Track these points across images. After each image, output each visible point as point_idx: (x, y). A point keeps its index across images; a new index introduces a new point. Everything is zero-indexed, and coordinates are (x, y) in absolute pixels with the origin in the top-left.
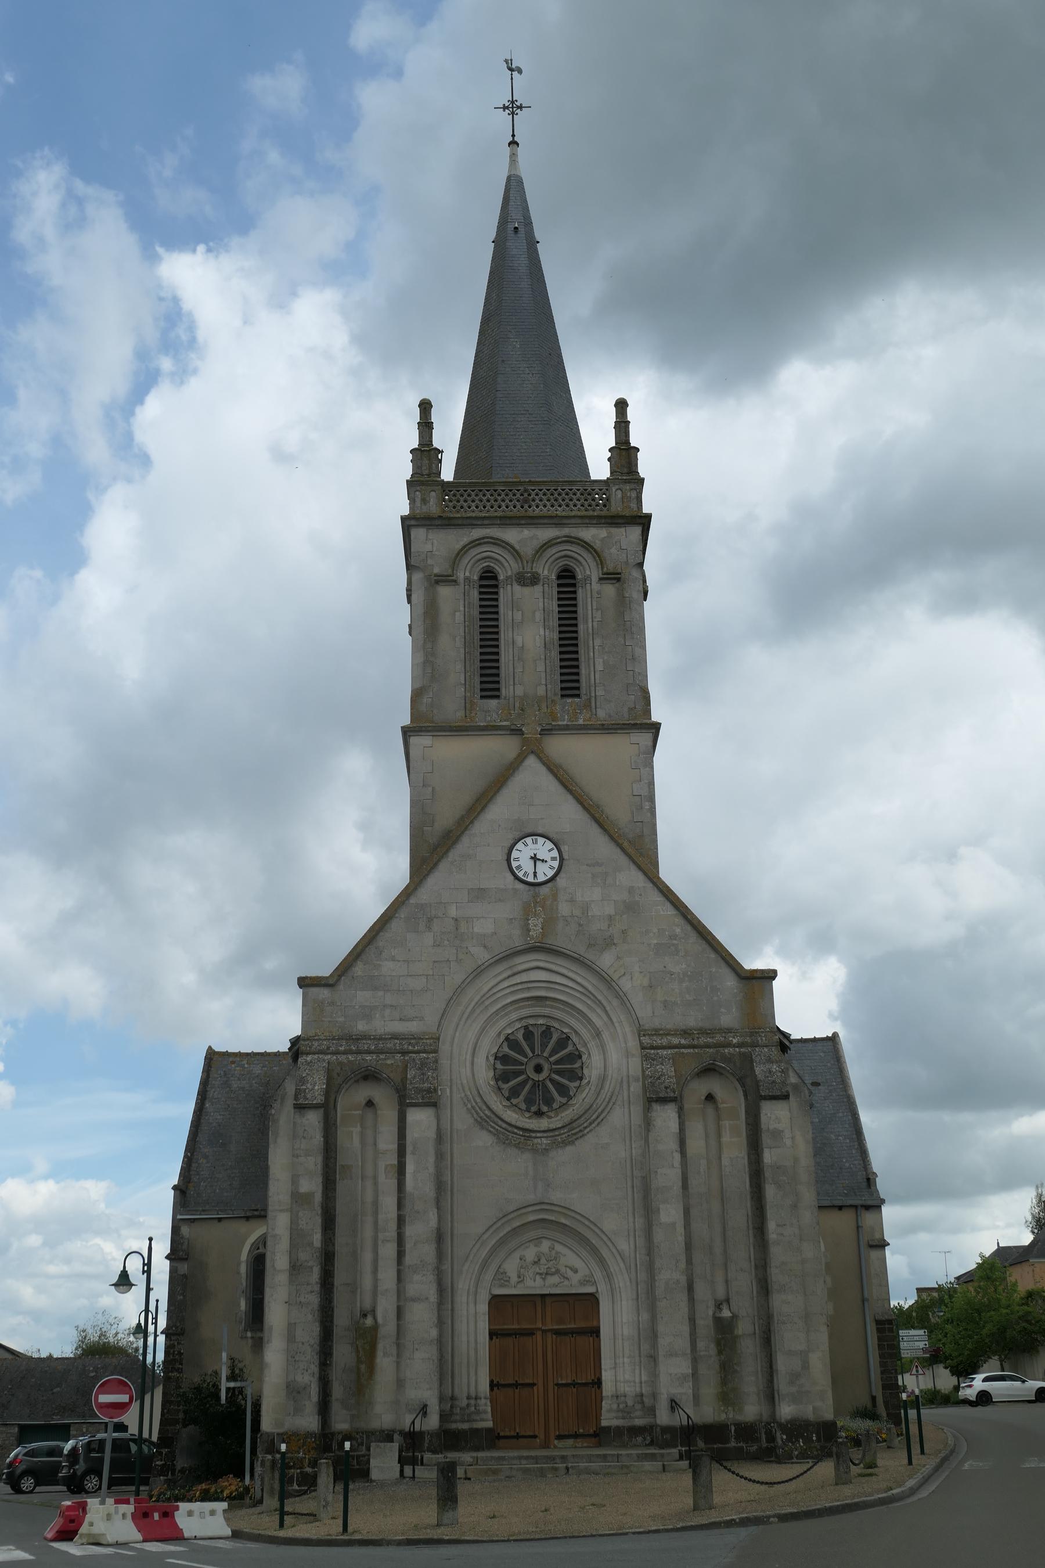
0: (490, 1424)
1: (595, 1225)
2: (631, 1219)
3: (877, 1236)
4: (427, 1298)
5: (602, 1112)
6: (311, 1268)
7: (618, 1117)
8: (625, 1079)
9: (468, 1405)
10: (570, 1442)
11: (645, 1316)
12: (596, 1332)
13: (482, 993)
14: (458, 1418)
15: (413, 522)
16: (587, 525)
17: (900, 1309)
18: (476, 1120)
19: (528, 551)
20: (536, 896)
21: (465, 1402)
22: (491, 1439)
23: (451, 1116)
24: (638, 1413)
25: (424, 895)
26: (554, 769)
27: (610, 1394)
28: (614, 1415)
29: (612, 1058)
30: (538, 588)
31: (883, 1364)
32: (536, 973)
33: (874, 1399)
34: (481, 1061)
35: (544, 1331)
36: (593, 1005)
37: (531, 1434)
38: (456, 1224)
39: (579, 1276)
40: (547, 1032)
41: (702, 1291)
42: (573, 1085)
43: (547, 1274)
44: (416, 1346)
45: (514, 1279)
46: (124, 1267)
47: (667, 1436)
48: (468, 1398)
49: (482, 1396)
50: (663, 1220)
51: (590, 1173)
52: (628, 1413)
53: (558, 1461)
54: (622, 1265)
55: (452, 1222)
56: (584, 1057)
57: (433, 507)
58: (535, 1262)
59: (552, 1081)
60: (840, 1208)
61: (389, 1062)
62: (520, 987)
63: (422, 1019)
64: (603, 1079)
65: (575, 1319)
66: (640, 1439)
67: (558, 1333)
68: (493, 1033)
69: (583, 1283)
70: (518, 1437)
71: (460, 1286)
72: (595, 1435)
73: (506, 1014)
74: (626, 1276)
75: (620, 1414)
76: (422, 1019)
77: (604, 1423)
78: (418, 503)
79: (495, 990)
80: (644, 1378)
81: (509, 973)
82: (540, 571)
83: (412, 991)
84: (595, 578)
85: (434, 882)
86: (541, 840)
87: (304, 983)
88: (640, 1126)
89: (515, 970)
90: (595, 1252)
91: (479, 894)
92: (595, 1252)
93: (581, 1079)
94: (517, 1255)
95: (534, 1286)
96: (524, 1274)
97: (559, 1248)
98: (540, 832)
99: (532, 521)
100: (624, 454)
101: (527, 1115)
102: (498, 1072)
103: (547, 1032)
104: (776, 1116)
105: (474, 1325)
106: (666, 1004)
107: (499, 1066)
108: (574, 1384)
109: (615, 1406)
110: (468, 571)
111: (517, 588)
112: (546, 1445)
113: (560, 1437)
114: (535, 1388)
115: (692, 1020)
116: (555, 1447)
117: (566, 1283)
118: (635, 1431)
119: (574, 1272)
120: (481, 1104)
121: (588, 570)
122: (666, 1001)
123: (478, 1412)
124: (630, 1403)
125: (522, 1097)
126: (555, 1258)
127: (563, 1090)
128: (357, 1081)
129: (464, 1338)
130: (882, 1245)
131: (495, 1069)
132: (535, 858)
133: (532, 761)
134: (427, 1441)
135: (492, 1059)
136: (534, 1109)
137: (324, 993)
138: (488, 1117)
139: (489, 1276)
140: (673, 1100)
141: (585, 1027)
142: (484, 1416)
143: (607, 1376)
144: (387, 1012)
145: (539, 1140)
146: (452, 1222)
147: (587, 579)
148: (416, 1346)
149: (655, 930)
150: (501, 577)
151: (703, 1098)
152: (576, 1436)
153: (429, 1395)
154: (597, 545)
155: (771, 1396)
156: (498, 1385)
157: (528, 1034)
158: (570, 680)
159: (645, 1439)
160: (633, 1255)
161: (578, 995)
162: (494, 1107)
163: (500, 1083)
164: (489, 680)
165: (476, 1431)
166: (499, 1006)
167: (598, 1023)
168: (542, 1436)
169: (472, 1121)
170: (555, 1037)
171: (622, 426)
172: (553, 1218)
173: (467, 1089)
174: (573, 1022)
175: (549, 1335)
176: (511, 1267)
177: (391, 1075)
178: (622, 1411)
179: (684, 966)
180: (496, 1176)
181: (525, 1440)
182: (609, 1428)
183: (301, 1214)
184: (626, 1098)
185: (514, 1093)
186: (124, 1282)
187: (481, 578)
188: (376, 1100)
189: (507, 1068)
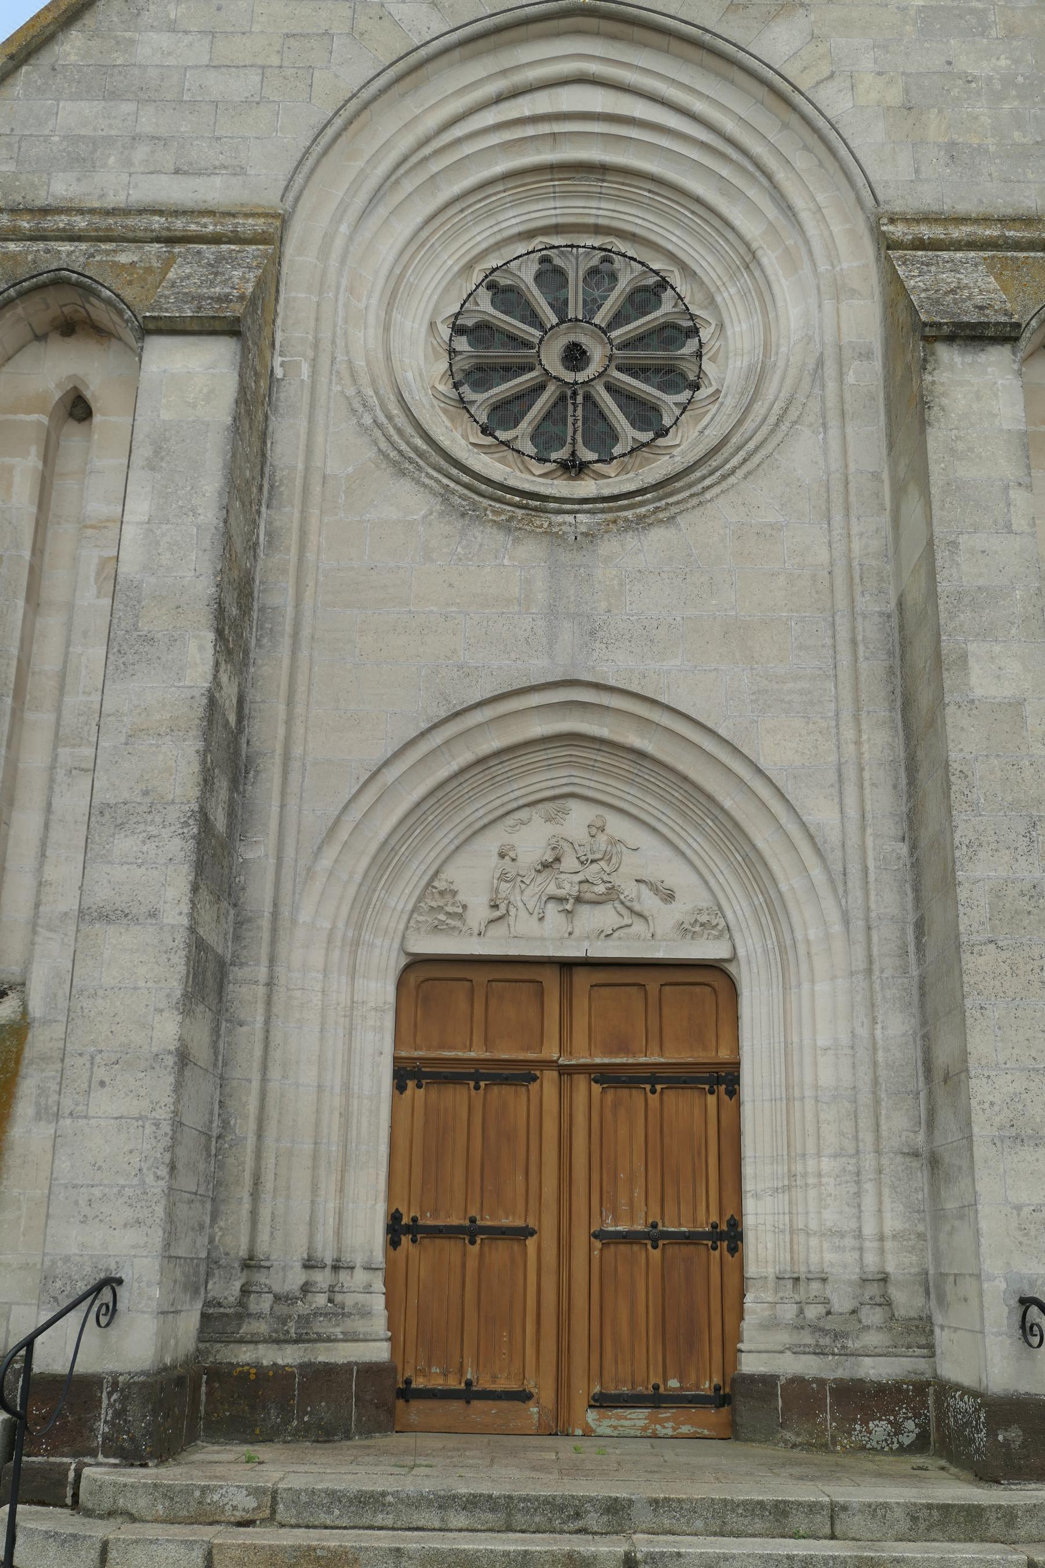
0: (379, 1352)
1: (736, 750)
2: (848, 733)
4: (153, 914)
5: (757, 449)
7: (804, 456)
8: (830, 352)
9: (306, 1289)
10: (637, 1418)
11: (896, 1026)
12: (725, 1079)
14: (262, 1327)
21: (296, 1278)
22: (376, 1403)
23: (310, 433)
24: (873, 1339)
27: (770, 1271)
28: (784, 1338)
35: (566, 1072)
37: (514, 1386)
38: (299, 730)
42: (669, 401)
43: (578, 900)
44: (100, 1073)
45: (479, 913)
47: (1011, 1435)
48: (310, 1264)
49: (359, 1260)
50: (978, 692)
51: (725, 600)
52: (837, 1336)
53: (593, 1520)
54: (817, 873)
55: (289, 722)
56: (705, 334)
58: (546, 866)
61: (124, 258)
62: (530, 131)
63: (240, 171)
64: (758, 378)
65: (665, 1036)
66: (880, 1429)
67: (608, 1077)
68: (451, 257)
69: (685, 931)
70: (468, 1394)
71: (305, 916)
72: (721, 1399)
74: (829, 905)
75: (808, 1339)
76: (240, 171)
77: (750, 1365)
79: (458, 131)
80: (892, 1223)
81: (500, 85)
83: (216, 103)
88: (876, 476)
90: (731, 833)
93: (696, 387)
94: (491, 842)
96: (506, 903)
97: (617, 826)
102: (462, 364)
105: (333, 1048)
106: (952, 152)
108: (654, 1237)
109: (789, 1312)
112: (557, 1426)
113: (603, 1402)
114: (531, 1242)
116: (588, 1433)
117: (639, 927)
118: (859, 1399)
119: (662, 899)
120: (401, 420)
122: (953, 144)
123: (338, 1312)
124: (842, 1303)
125: (526, 426)
126: (607, 857)
127: (645, 414)
128: (40, 337)
129: (309, 1075)
131: (452, 352)
134: (106, 1413)
135: (445, 331)
136: (562, 454)
138: (421, 454)
141: (711, 248)
142: (358, 1325)
143: (759, 1214)
144: (141, 152)
145: (569, 518)
146: (289, 722)
148: (100, 1073)
152: (656, 1400)
153: (131, 1244)
156: (415, 1229)
159: (898, 1429)
160: (853, 839)
161: (694, 154)
162: (444, 441)
163: (465, 389)
165: (323, 1377)
168: (547, 1395)
169: (371, 453)
170: (624, 282)
172: (605, 732)
173: (364, 380)
174: (674, 238)
175: (581, 1083)
176: (473, 877)
177: (128, 294)
178: (816, 1329)
179: (1003, 62)
180: (418, 599)
181: (493, 1408)
182: (768, 1381)
184: (832, 401)
185: (505, 413)
188: (95, 390)
189: (488, 353)
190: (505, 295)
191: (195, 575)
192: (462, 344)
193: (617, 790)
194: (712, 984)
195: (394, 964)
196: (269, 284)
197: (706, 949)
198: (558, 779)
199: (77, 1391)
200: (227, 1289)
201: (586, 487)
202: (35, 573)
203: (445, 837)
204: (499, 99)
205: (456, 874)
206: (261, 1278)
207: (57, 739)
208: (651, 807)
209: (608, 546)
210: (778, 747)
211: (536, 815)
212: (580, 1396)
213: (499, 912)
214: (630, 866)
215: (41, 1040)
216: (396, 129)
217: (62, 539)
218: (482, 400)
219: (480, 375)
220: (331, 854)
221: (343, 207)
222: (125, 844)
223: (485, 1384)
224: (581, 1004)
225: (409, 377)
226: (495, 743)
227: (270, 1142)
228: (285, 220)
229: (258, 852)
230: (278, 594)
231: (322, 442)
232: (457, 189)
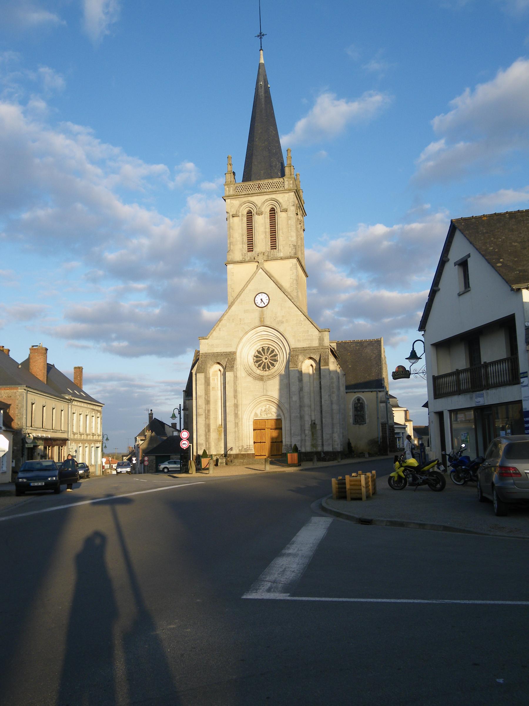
17: (336, 424)
20: (262, 311)
30: (263, 216)
45: (259, 415)
46: (413, 348)
91: (246, 311)
97: (271, 407)
99: (261, 194)
121: (278, 210)
143: (284, 440)
155: (323, 445)
157: (263, 350)
158: (274, 245)
185: (259, 366)
189: (258, 359)
192: (255, 358)
195: (253, 420)
209: (268, 382)
218: (257, 364)
219: (257, 362)
225: (250, 364)
229: (239, 413)
231: (241, 373)
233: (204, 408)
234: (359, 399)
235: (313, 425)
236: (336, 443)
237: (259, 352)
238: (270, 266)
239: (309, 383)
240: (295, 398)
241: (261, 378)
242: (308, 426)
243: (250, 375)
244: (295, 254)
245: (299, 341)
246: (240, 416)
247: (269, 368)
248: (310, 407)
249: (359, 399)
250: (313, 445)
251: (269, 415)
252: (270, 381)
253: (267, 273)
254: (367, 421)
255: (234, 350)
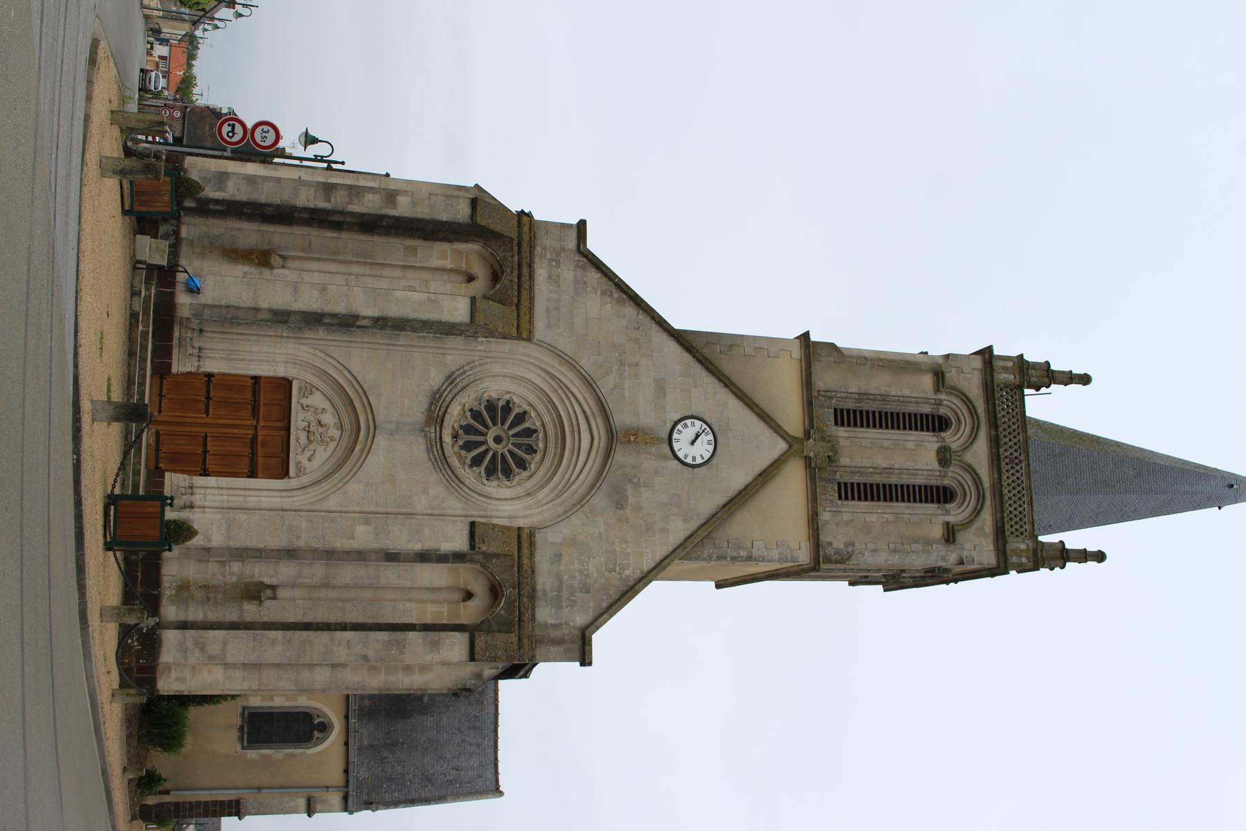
0: (174, 369)
3: (319, 806)
6: (330, 201)
7: (454, 505)
12: (253, 474)
13: (570, 386)
15: (987, 356)
16: (994, 514)
18: (453, 373)
19: (969, 457)
20: (659, 439)
21: (197, 345)
25: (659, 337)
26: (775, 466)
29: (507, 504)
30: (936, 466)
31: (198, 803)
32: (589, 439)
33: (167, 792)
34: (507, 385)
35: (256, 427)
36: (556, 491)
39: (305, 462)
40: (531, 450)
41: (285, 571)
45: (305, 402)
48: (200, 349)
57: (1003, 377)
58: (320, 422)
59: (487, 451)
60: (346, 771)
65: (266, 455)
67: (254, 439)
68: (532, 398)
69: (299, 463)
70: (161, 396)
71: (302, 347)
72: (157, 467)
73: (549, 411)
78: (1001, 363)
79: (572, 399)
81: (589, 413)
82: (952, 468)
84: (948, 519)
85: (672, 347)
86: (711, 448)
87: (582, 225)
89: (591, 418)
90: (328, 476)
91: (660, 389)
92: (328, 476)
94: (328, 406)
95: (298, 420)
96: (311, 410)
97: (333, 445)
98: (719, 448)
100: (1062, 556)
101: (456, 426)
103: (531, 450)
104: (455, 647)
105: (264, 357)
107: (501, 403)
108: (205, 452)
110: (949, 405)
111: (935, 446)
113: (158, 434)
115: (544, 581)
121: (956, 513)
126: (322, 441)
128: (492, 267)
129: (255, 349)
130: (310, 812)
132: (692, 445)
133: (782, 446)
137: (572, 244)
139: (311, 379)
140: (472, 547)
143: (211, 481)
147: (948, 513)
149: (629, 550)
150: (943, 434)
151: (469, 588)
152: (157, 449)
154: (977, 524)
155: (184, 626)
156: (209, 381)
157: (530, 432)
164: (849, 417)
166: (556, 402)
167: (541, 495)
168: (159, 418)
169: (453, 369)
171: (1083, 556)
174: (541, 473)
175: (252, 432)
176: (317, 400)
180: (400, 382)
183: (378, 196)
186: (310, 140)
187: (940, 418)
189: (498, 411)
190: (522, 417)
191: (394, 311)
193: (344, 445)
194: (284, 473)
196: (523, 339)
197: (292, 470)
198: (347, 426)
199: (172, 284)
200: (195, 323)
201: (447, 439)
202: (413, 267)
203: (329, 391)
204: (584, 412)
205: (318, 394)
206: (196, 334)
207: (357, 275)
208: (338, 454)
209: (422, 441)
210: (352, 487)
211: (336, 420)
212: (162, 428)
213: (305, 408)
214: (320, 449)
215: (266, 272)
216: (568, 377)
217: (425, 275)
220: (322, 355)
221: (541, 361)
222: (316, 293)
223: (164, 401)
224: (277, 433)
226: (357, 405)
227: (235, 337)
228: (529, 339)
229: (321, 333)
230: (404, 339)
231: (456, 353)
232: (554, 399)
233: (351, 208)
234: (324, 728)
235: (255, 592)
236: (188, 675)
237: (522, 417)
238: (792, 486)
239: (408, 584)
240: (363, 537)
241: (435, 417)
242: (260, 572)
243: (450, 379)
244: (828, 560)
245: (558, 557)
246: (308, 334)
247: (468, 446)
248: (326, 585)
249: (324, 728)
250: (184, 587)
251: (303, 436)
252: (423, 448)
253: (765, 477)
254: (253, 754)
255: (541, 330)
